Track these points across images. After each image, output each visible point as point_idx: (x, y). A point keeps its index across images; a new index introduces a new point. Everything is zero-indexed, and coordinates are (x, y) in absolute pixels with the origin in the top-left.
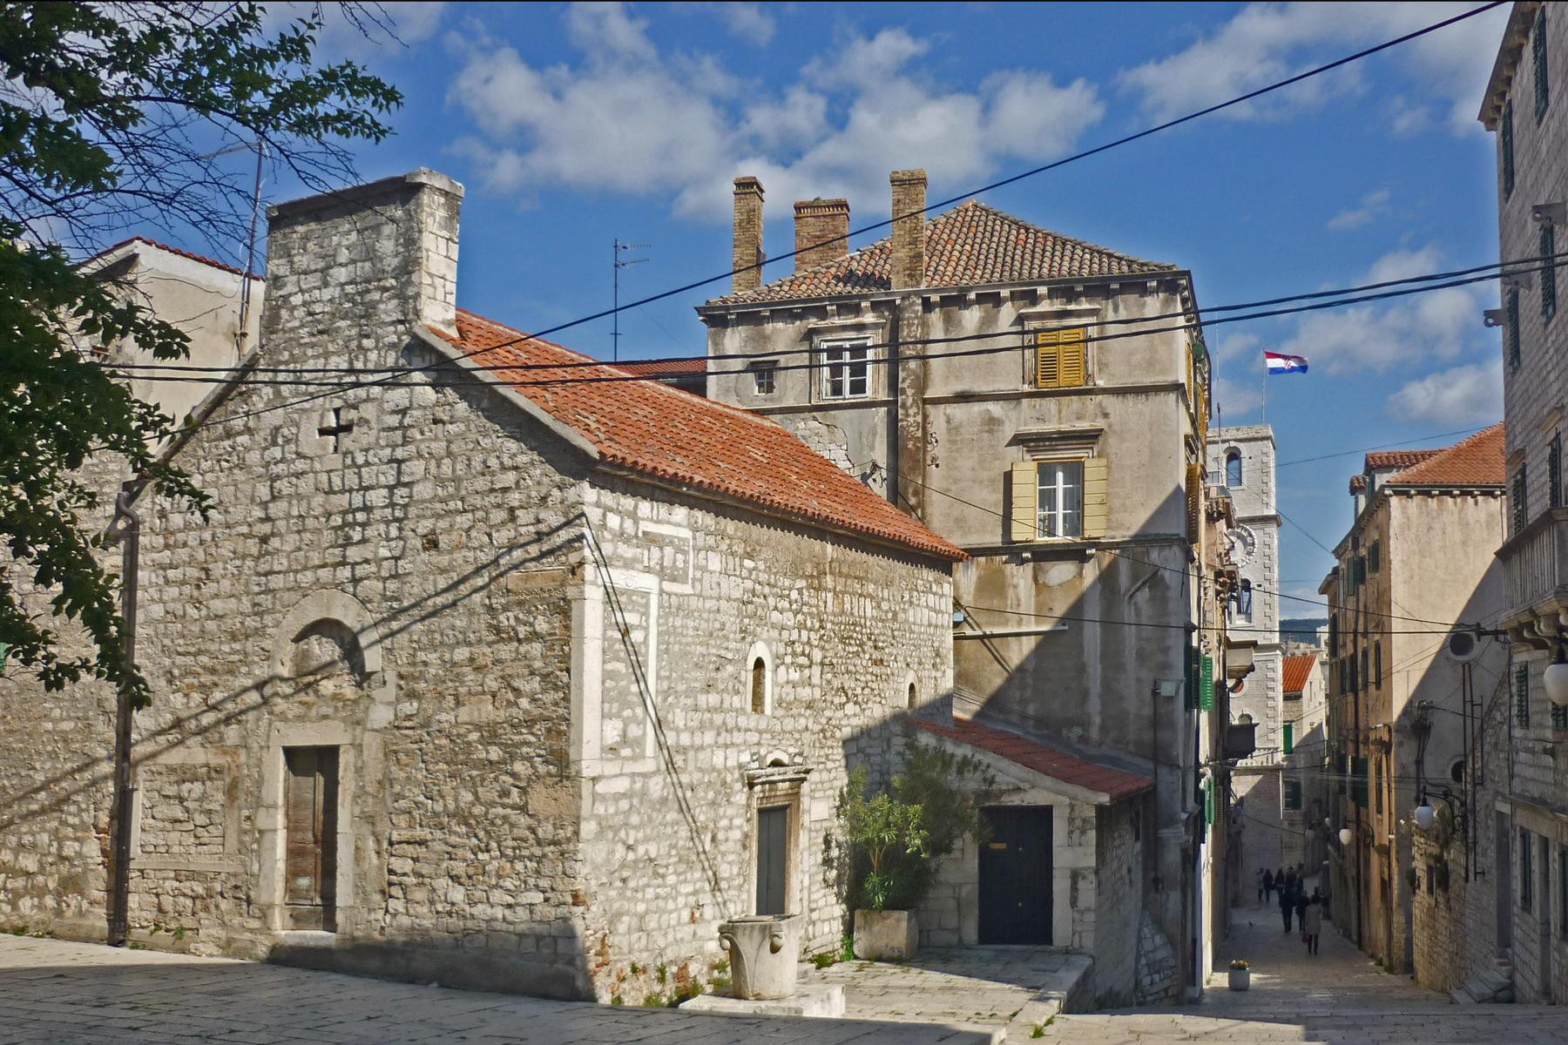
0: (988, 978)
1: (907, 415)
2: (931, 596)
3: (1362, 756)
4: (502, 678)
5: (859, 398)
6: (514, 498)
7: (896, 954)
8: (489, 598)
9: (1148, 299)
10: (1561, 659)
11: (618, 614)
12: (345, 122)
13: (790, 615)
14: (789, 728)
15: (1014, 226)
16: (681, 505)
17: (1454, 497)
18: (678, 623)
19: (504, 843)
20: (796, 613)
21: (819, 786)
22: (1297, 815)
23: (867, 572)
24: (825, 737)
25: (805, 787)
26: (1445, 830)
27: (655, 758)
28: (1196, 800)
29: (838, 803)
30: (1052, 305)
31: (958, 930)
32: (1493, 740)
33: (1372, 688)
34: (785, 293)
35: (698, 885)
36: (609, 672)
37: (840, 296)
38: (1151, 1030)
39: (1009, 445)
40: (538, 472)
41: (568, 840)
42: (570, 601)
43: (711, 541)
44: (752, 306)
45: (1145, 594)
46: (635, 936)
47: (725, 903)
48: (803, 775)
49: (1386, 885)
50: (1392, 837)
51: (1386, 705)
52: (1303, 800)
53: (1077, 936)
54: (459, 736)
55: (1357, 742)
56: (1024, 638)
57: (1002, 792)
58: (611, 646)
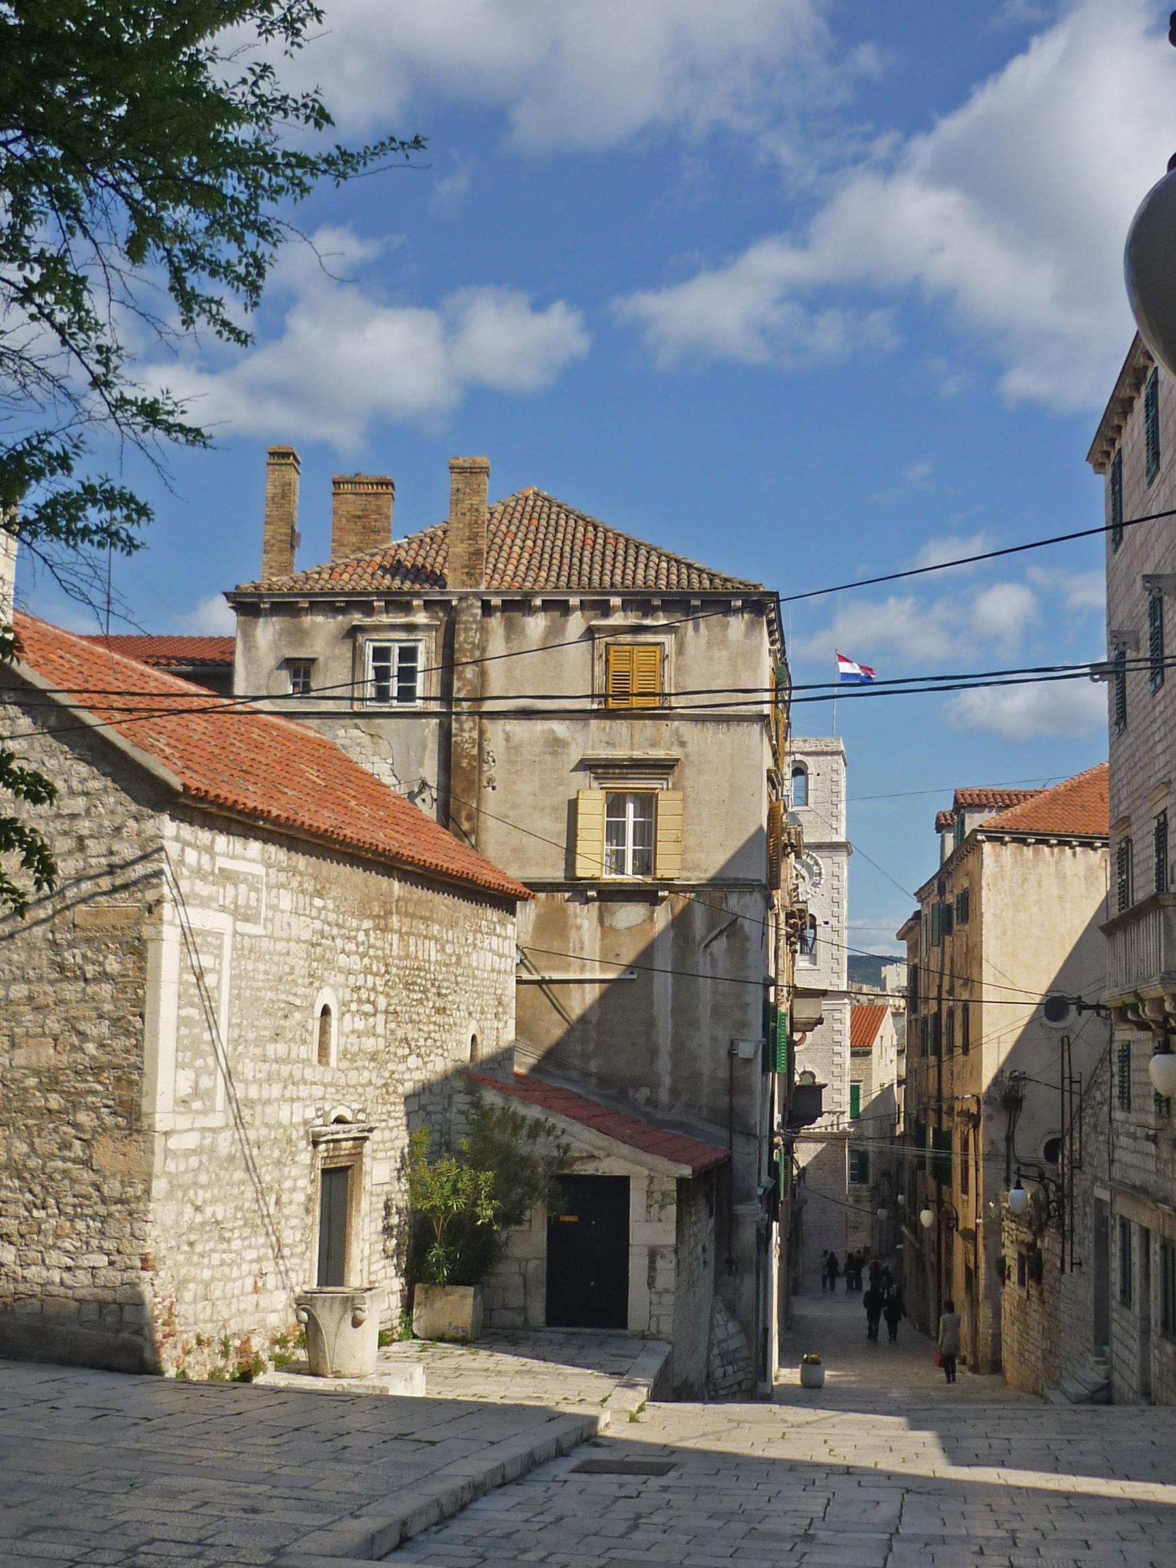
0: (565, 1363)
1: (462, 730)
2: (495, 938)
3: (945, 1128)
4: (66, 1020)
5: (407, 707)
6: (84, 826)
7: (460, 1334)
8: (52, 932)
9: (732, 620)
10: (1164, 1048)
11: (194, 956)
12: (109, 535)
13: (357, 958)
14: (352, 1082)
15: (580, 522)
16: (256, 839)
17: (1051, 846)
18: (250, 966)
19: (64, 1200)
20: (363, 956)
21: (381, 1146)
22: (864, 1190)
23: (432, 911)
24: (387, 1093)
25: (368, 1146)
26: (1039, 1216)
27: (225, 1111)
28: (769, 1175)
29: (399, 1165)
30: (626, 617)
31: (524, 1309)
32: (1093, 1120)
33: (958, 1051)
34: (324, 583)
35: (263, 1251)
36: (183, 1018)
37: (389, 592)
38: (750, 1419)
39: (575, 769)
40: (112, 799)
41: (138, 1199)
42: (146, 941)
43: (283, 877)
44: (289, 595)
45: (722, 942)
46: (201, 1305)
47: (287, 1271)
48: (366, 1134)
49: (971, 1274)
50: (980, 1221)
51: (975, 1074)
52: (871, 1171)
53: (654, 1319)
54: (13, 1080)
55: (939, 1112)
56: (587, 986)
57: (576, 1159)
58: (186, 990)
